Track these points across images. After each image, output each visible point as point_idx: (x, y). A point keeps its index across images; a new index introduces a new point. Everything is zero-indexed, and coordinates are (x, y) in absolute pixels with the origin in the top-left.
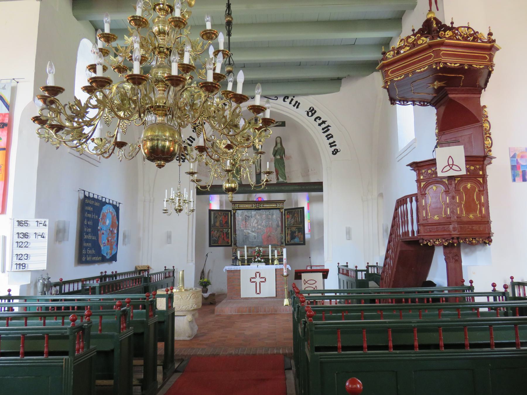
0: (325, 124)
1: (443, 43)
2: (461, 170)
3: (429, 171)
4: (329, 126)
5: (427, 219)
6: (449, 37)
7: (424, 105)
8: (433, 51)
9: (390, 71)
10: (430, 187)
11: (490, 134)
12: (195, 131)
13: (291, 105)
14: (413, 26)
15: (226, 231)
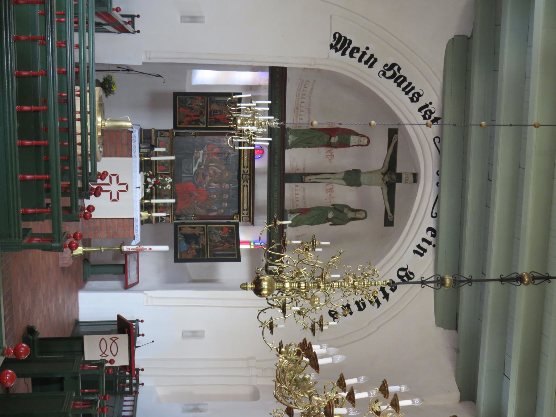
0: (384, 298)
4: (379, 304)
12: (386, 68)
13: (420, 242)
15: (202, 121)
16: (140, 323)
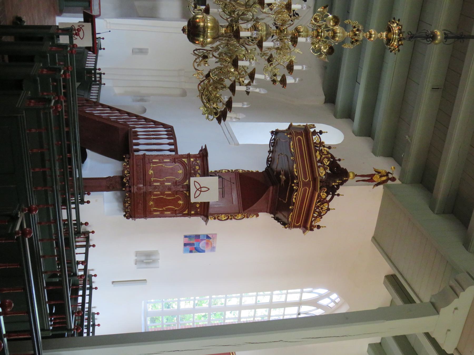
1: (316, 191)
2: (195, 198)
3: (197, 167)
5: (150, 163)
6: (321, 195)
7: (268, 161)
8: (310, 182)
9: (302, 138)
10: (181, 167)
11: (231, 219)
14: (344, 159)
16: (102, 40)
